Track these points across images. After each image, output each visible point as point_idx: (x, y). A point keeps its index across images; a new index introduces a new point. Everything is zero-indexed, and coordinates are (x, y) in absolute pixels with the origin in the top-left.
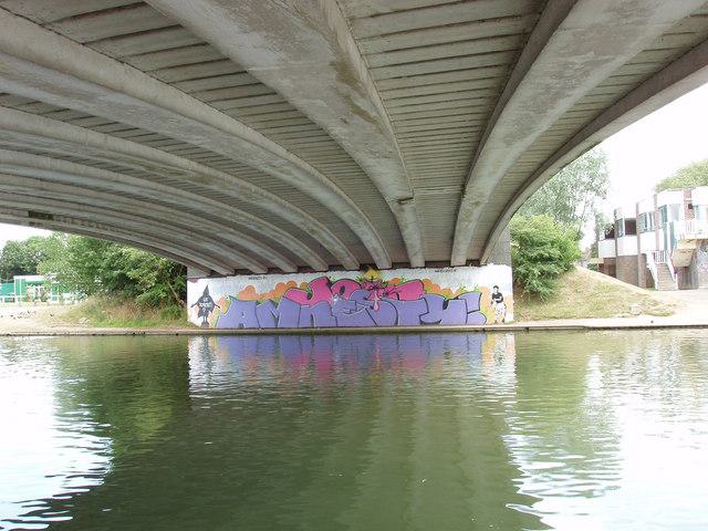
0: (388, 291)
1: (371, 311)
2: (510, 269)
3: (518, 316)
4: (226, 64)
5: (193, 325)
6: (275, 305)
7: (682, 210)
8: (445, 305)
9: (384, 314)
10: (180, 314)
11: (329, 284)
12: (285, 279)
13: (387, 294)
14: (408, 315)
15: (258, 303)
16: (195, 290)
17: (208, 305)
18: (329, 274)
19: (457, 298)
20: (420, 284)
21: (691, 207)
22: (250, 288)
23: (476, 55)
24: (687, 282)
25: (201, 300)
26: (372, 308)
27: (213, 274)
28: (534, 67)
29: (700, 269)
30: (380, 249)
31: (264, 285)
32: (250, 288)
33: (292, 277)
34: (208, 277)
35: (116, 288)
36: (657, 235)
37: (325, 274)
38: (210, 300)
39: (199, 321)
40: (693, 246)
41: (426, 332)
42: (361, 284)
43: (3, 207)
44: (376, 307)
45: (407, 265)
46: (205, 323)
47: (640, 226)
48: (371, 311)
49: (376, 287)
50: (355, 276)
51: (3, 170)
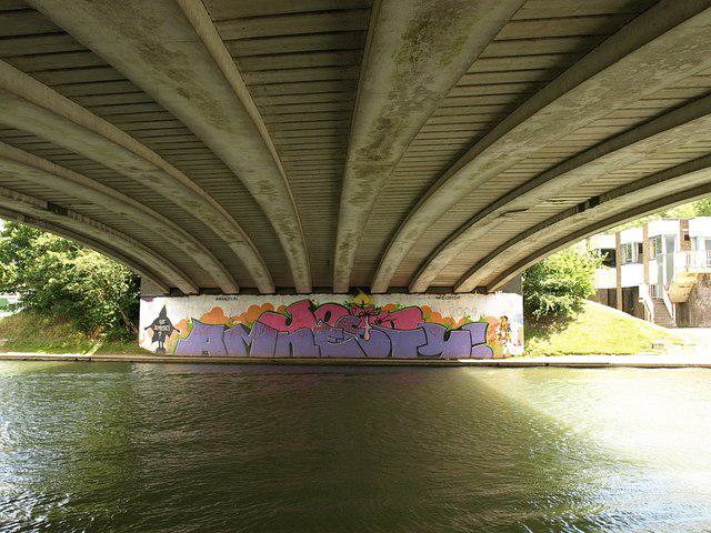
0: (381, 318)
1: (361, 341)
2: (521, 298)
3: (528, 352)
4: (61, 38)
5: (148, 353)
6: (248, 330)
7: (678, 242)
8: (447, 336)
9: (374, 344)
10: (132, 337)
11: (313, 308)
12: (259, 301)
13: (380, 322)
14: (405, 348)
15: (226, 327)
16: (149, 311)
17: (165, 328)
18: (312, 297)
19: (460, 329)
20: (419, 311)
21: (687, 238)
22: (218, 311)
23: (302, 53)
24: (682, 319)
25: (156, 322)
26: (362, 337)
27: (173, 292)
28: (695, 18)
29: (699, 305)
30: (392, 272)
31: (235, 308)
32: (218, 311)
33: (269, 299)
34: (167, 295)
35: (39, 309)
36: (646, 271)
37: (307, 297)
38: (168, 322)
39: (152, 347)
40: (694, 280)
41: (422, 366)
42: (351, 309)
43: (12, 189)
44: (367, 337)
45: (329, 290)
46: (161, 349)
47: (621, 257)
48: (361, 341)
49: (368, 312)
50: (341, 300)
51: (18, 117)
